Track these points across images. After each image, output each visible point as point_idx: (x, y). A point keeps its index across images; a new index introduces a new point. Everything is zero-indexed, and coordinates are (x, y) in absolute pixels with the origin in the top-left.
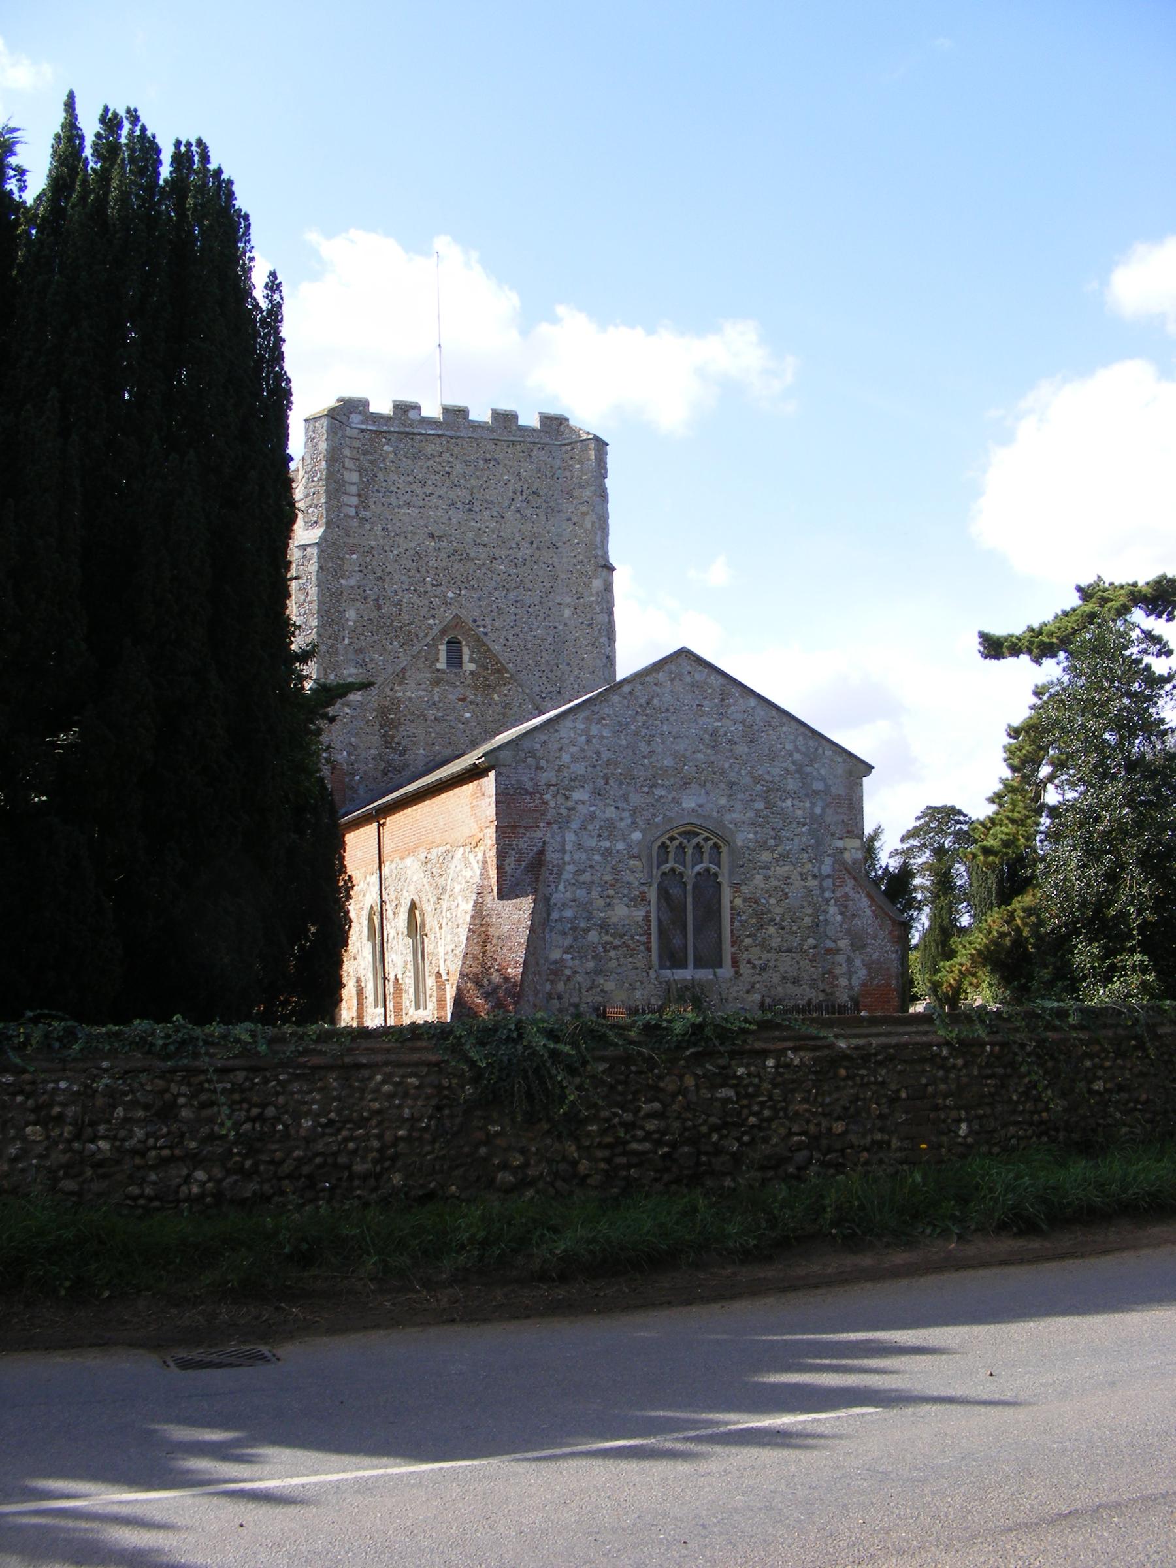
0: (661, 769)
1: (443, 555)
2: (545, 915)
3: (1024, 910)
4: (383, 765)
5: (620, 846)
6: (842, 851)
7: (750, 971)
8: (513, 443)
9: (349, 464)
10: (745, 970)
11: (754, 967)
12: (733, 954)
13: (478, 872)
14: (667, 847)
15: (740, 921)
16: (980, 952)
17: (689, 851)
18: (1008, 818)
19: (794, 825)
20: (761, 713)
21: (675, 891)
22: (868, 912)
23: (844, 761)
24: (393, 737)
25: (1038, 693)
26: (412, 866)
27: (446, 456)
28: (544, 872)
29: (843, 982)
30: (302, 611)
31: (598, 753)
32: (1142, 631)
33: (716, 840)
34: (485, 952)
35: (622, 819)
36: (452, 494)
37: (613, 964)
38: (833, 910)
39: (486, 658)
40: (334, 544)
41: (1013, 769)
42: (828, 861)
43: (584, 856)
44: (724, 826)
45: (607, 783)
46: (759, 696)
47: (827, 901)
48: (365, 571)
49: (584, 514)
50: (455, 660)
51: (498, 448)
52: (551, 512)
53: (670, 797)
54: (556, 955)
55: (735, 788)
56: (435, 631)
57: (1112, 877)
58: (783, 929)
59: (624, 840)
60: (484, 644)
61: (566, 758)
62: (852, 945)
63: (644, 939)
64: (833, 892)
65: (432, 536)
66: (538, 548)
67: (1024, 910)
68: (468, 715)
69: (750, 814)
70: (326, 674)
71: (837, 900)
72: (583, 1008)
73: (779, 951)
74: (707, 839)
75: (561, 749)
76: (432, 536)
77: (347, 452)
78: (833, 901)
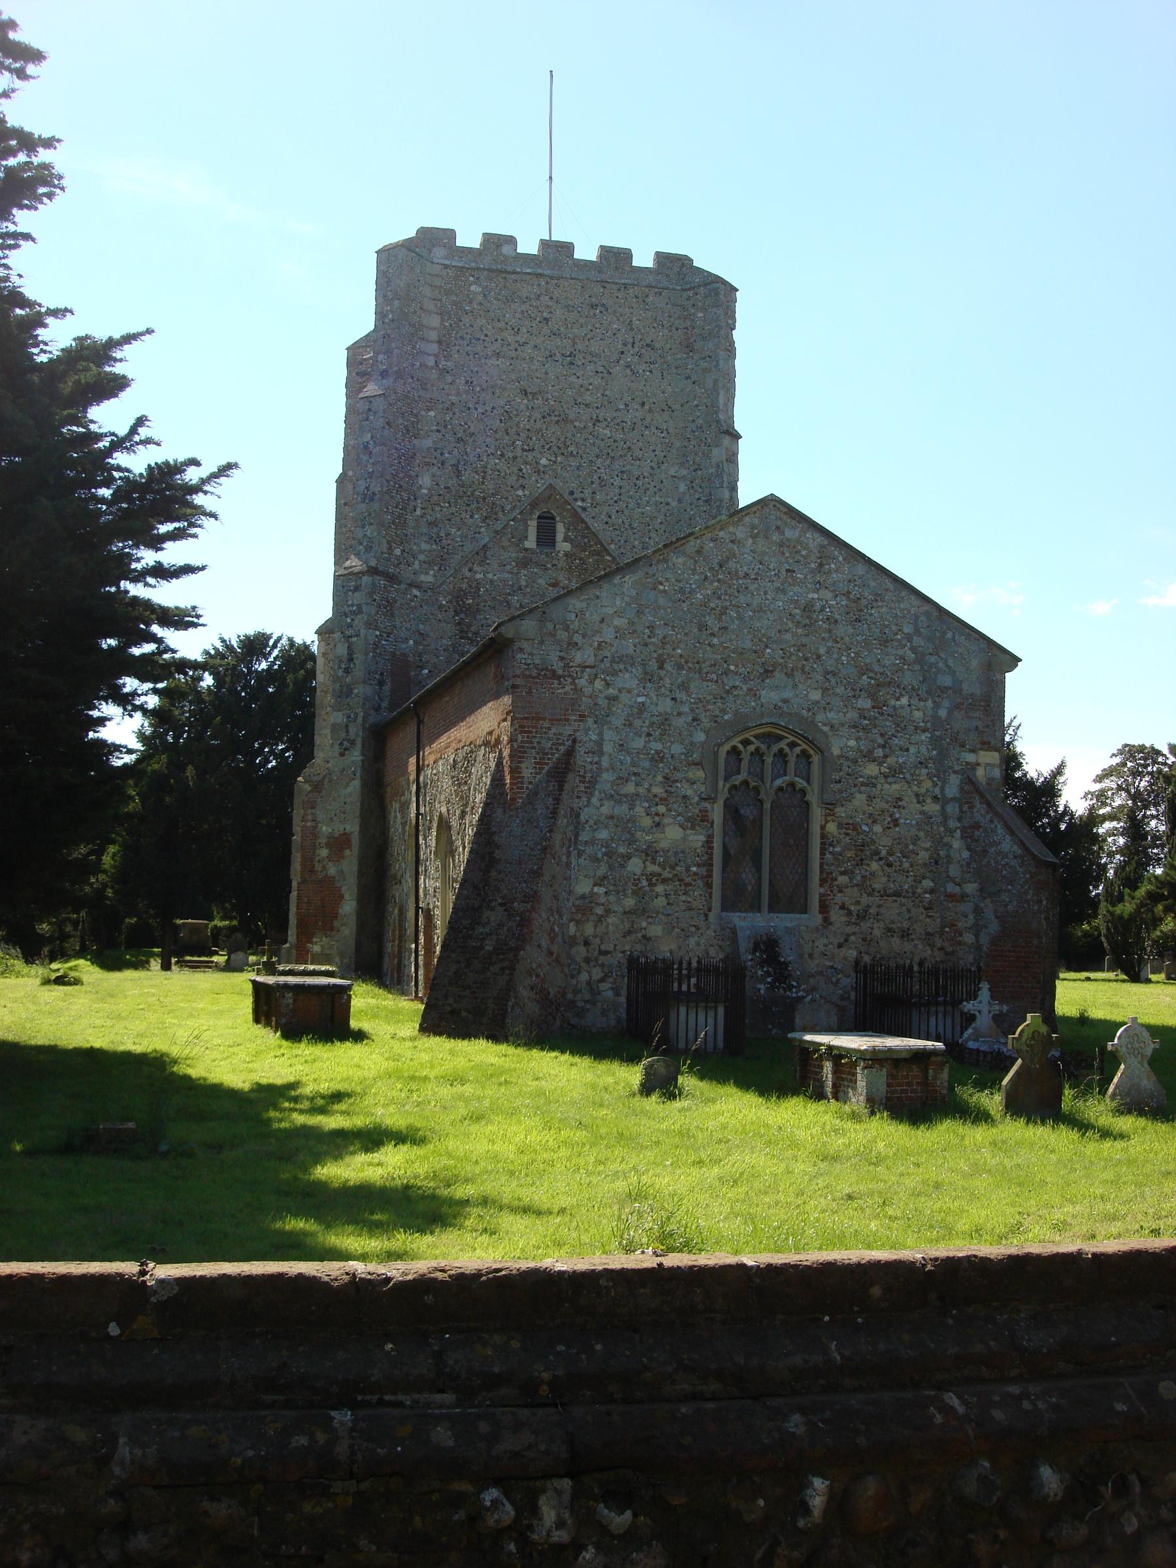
5: (677, 749)
6: (974, 766)
7: (844, 919)
10: (836, 915)
11: (850, 913)
17: (769, 760)
21: (748, 812)
24: (469, 626)
27: (545, 299)
31: (651, 627)
33: (804, 746)
42: (955, 780)
45: (661, 667)
50: (546, 537)
54: (583, 887)
58: (890, 865)
60: (583, 521)
61: (608, 635)
62: (981, 890)
64: (960, 820)
66: (650, 411)
69: (852, 715)
70: (390, 548)
73: (884, 894)
74: (792, 745)
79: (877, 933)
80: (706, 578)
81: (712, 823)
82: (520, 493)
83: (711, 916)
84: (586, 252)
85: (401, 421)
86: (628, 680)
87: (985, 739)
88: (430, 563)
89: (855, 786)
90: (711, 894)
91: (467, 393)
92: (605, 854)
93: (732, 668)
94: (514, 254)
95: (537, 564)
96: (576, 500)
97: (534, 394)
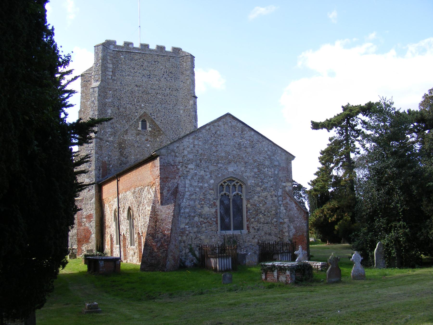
1: (140, 92)
2: (178, 211)
3: (327, 208)
4: (120, 162)
5: (206, 185)
9: (109, 61)
10: (252, 230)
11: (255, 229)
12: (247, 225)
13: (153, 195)
14: (223, 186)
15: (250, 213)
16: (313, 223)
17: (231, 187)
18: (322, 180)
19: (268, 177)
20: (256, 137)
21: (226, 202)
22: (295, 209)
23: (285, 155)
24: (123, 153)
25: (330, 140)
26: (129, 194)
27: (142, 60)
28: (178, 195)
29: (286, 234)
30: (93, 110)
31: (198, 151)
32: (362, 120)
34: (156, 225)
35: (206, 175)
36: (143, 72)
37: (204, 229)
38: (282, 208)
40: (104, 87)
41: (323, 164)
42: (280, 190)
43: (193, 189)
44: (244, 178)
45: (201, 162)
46: (255, 131)
47: (280, 205)
50: (144, 127)
51: (159, 58)
52: (176, 79)
54: (182, 226)
55: (247, 164)
56: (138, 117)
57: (389, 193)
58: (265, 215)
60: (154, 122)
63: (215, 219)
64: (282, 202)
67: (327, 208)
68: (148, 145)
69: (253, 174)
71: (283, 204)
72: (193, 246)
74: (237, 183)
75: (184, 149)
77: (108, 57)
78: (282, 205)
79: (263, 234)
82: (136, 114)
83: (218, 232)
84: (153, 47)
88: (111, 135)
92: (188, 216)
95: (142, 134)
97: (139, 86)
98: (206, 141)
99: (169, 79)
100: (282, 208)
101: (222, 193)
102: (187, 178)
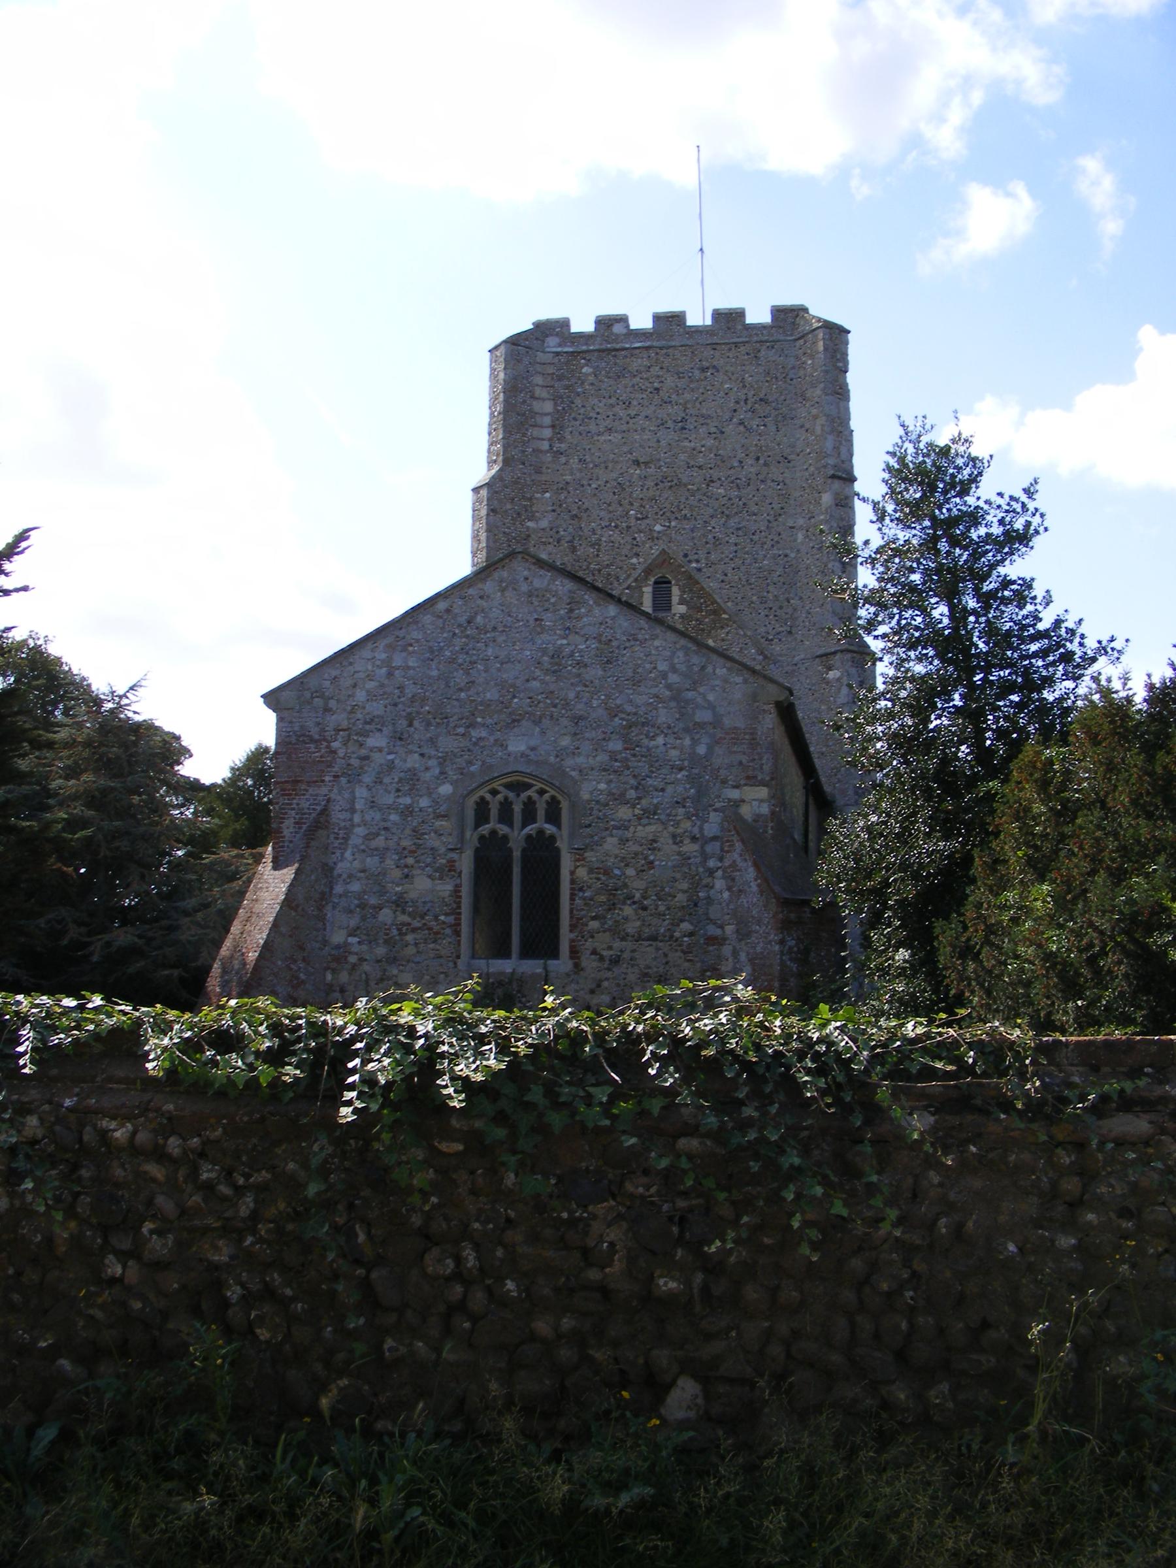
0: (481, 703)
5: (424, 802)
7: (595, 964)
8: (736, 345)
10: (589, 963)
11: (602, 959)
12: (572, 941)
15: (584, 899)
22: (754, 888)
23: (745, 681)
27: (655, 370)
31: (401, 688)
33: (553, 792)
37: (411, 950)
38: (719, 884)
39: (699, 598)
40: (516, 483)
42: (715, 818)
43: (378, 816)
45: (410, 725)
47: (711, 872)
48: (559, 510)
49: (815, 417)
51: (717, 354)
53: (492, 739)
54: (338, 938)
58: (645, 908)
59: (430, 794)
61: (360, 696)
64: (721, 859)
65: (637, 463)
66: (766, 464)
69: (602, 758)
73: (639, 938)
74: (542, 792)
75: (355, 686)
76: (637, 463)
78: (720, 873)
79: (632, 977)
80: (455, 634)
81: (460, 873)
82: (634, 560)
83: (459, 962)
84: (758, 315)
85: (509, 506)
86: (376, 741)
87: (750, 773)
89: (607, 829)
90: (459, 941)
91: (580, 471)
92: (358, 906)
93: (479, 720)
94: (625, 331)
96: (690, 562)
97: (646, 464)
98: (432, 652)
99: (754, 423)
100: (719, 884)
101: (527, 829)
102: (360, 781)
